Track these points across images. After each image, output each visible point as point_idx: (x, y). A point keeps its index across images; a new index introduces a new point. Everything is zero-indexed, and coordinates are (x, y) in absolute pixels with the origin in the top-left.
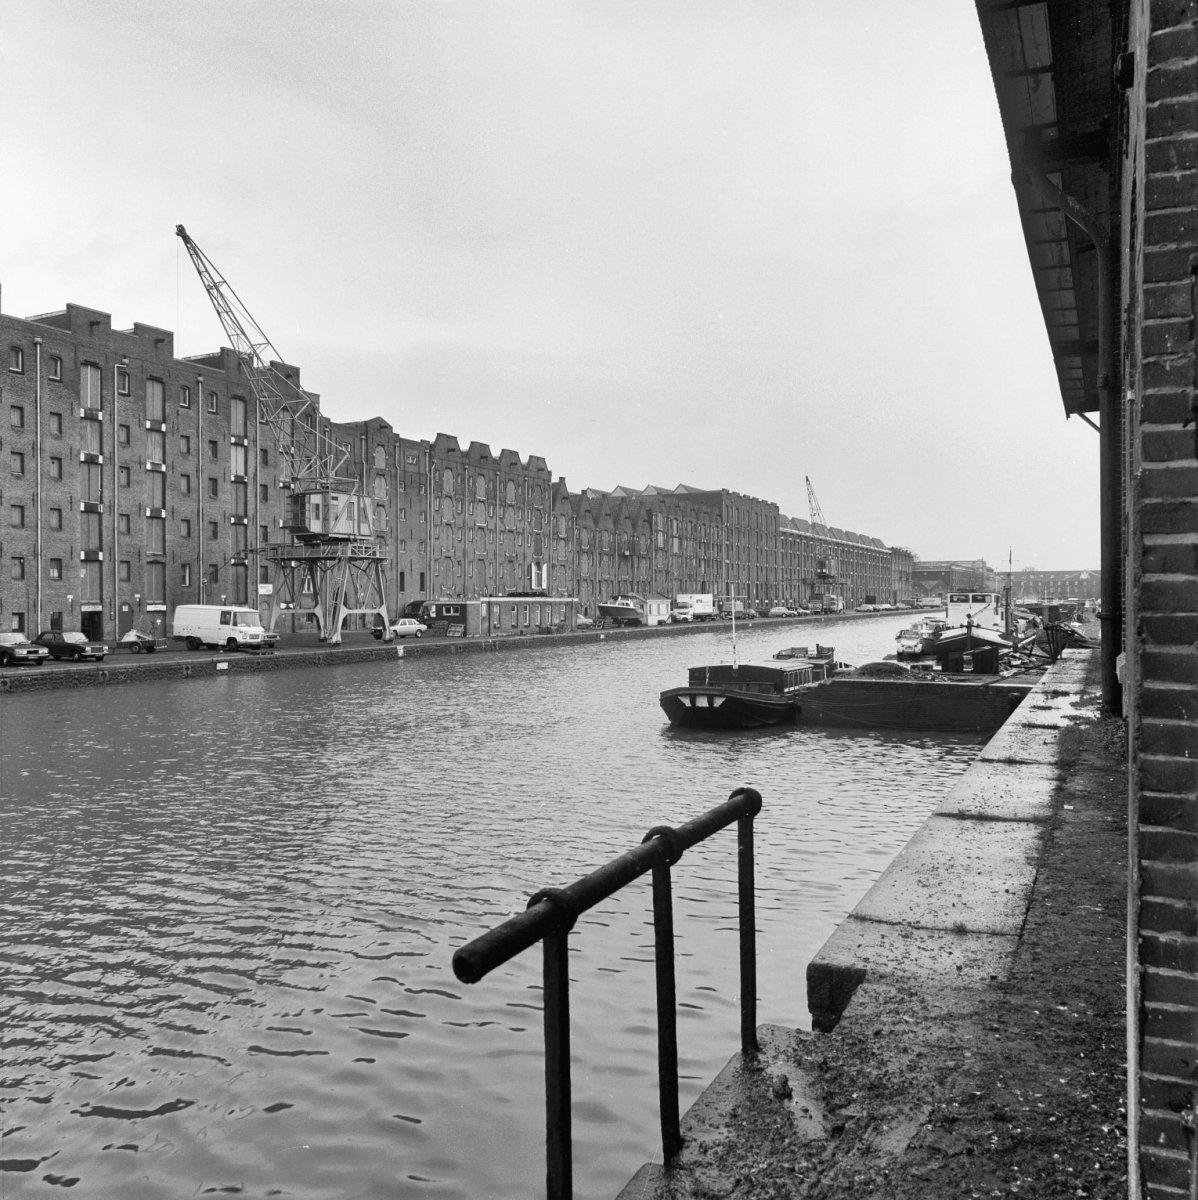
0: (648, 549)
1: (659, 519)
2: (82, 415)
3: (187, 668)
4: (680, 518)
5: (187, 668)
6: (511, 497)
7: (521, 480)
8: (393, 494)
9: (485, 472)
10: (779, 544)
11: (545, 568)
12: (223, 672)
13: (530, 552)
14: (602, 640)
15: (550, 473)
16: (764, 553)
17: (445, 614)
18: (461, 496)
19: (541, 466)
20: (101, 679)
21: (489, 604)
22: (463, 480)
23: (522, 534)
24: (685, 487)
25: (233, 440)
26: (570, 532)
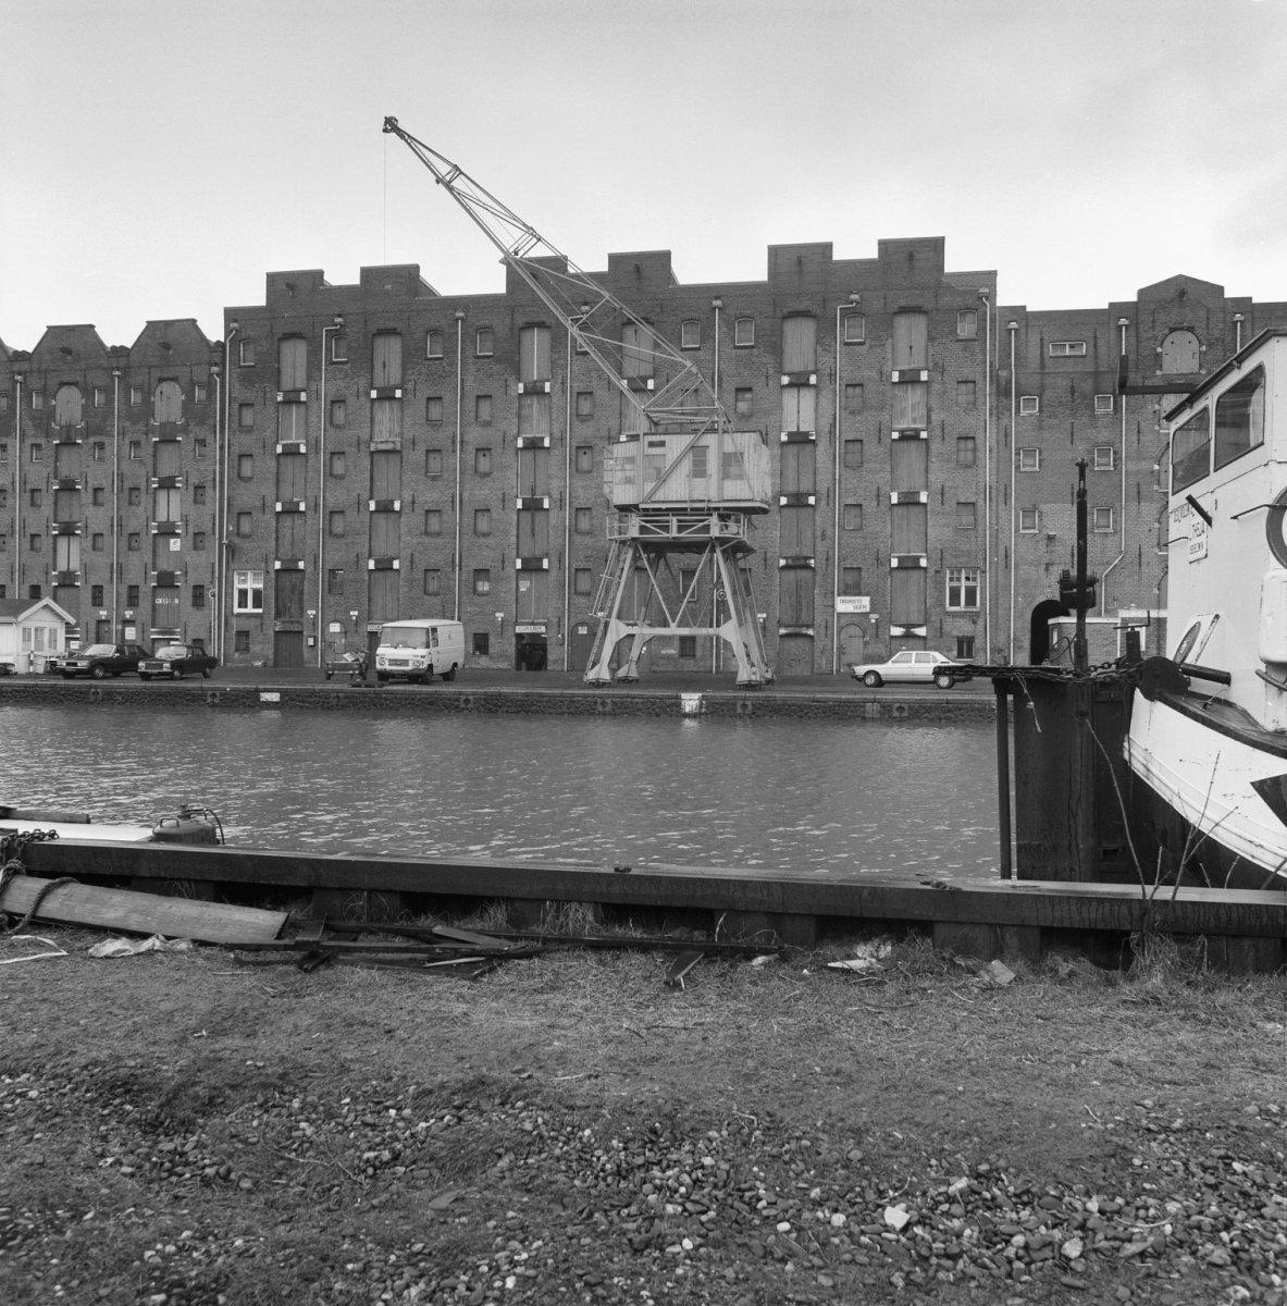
2: (521, 391)
3: (214, 695)
5: (214, 695)
20: (92, 698)
25: (785, 380)
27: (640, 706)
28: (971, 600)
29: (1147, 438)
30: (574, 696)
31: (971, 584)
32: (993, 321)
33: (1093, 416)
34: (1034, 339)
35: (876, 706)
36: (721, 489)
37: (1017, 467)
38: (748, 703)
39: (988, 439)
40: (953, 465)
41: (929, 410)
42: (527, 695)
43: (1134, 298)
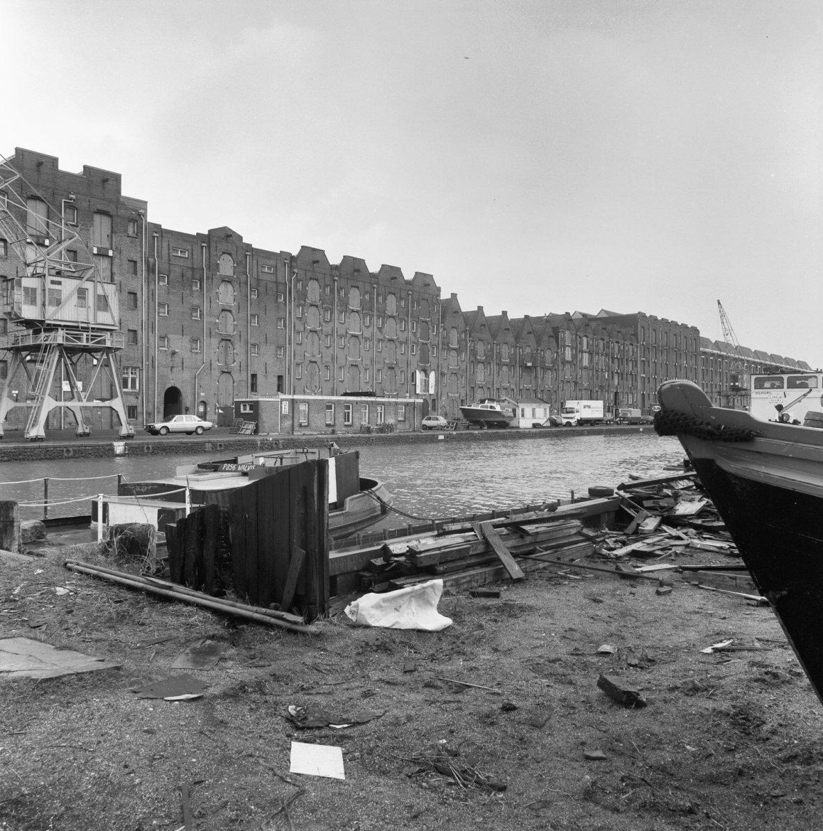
0: (554, 362)
1: (567, 336)
4: (591, 336)
6: (354, 304)
7: (404, 294)
8: (242, 301)
9: (359, 284)
10: (700, 362)
11: (432, 375)
12: (441, 441)
13: (415, 360)
14: (641, 432)
15: (439, 289)
16: (710, 373)
17: (242, 411)
18: (326, 305)
19: (428, 281)
21: (293, 402)
22: (332, 291)
23: (332, 335)
24: (606, 312)
26: (463, 343)
27: (90, 452)
28: (133, 386)
29: (213, 305)
30: (47, 447)
31: (134, 376)
32: (146, 229)
33: (191, 290)
34: (165, 245)
35: (210, 445)
36: (95, 316)
37: (159, 313)
38: (71, 449)
39: (143, 298)
40: (126, 307)
41: (112, 274)
42: (15, 448)
43: (206, 233)
